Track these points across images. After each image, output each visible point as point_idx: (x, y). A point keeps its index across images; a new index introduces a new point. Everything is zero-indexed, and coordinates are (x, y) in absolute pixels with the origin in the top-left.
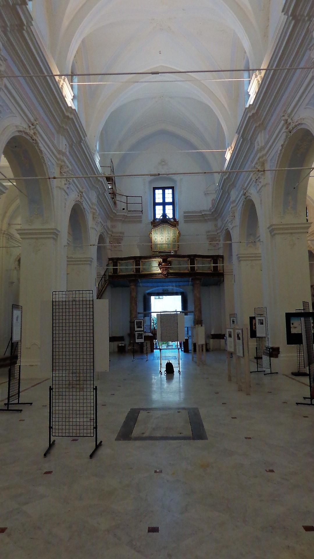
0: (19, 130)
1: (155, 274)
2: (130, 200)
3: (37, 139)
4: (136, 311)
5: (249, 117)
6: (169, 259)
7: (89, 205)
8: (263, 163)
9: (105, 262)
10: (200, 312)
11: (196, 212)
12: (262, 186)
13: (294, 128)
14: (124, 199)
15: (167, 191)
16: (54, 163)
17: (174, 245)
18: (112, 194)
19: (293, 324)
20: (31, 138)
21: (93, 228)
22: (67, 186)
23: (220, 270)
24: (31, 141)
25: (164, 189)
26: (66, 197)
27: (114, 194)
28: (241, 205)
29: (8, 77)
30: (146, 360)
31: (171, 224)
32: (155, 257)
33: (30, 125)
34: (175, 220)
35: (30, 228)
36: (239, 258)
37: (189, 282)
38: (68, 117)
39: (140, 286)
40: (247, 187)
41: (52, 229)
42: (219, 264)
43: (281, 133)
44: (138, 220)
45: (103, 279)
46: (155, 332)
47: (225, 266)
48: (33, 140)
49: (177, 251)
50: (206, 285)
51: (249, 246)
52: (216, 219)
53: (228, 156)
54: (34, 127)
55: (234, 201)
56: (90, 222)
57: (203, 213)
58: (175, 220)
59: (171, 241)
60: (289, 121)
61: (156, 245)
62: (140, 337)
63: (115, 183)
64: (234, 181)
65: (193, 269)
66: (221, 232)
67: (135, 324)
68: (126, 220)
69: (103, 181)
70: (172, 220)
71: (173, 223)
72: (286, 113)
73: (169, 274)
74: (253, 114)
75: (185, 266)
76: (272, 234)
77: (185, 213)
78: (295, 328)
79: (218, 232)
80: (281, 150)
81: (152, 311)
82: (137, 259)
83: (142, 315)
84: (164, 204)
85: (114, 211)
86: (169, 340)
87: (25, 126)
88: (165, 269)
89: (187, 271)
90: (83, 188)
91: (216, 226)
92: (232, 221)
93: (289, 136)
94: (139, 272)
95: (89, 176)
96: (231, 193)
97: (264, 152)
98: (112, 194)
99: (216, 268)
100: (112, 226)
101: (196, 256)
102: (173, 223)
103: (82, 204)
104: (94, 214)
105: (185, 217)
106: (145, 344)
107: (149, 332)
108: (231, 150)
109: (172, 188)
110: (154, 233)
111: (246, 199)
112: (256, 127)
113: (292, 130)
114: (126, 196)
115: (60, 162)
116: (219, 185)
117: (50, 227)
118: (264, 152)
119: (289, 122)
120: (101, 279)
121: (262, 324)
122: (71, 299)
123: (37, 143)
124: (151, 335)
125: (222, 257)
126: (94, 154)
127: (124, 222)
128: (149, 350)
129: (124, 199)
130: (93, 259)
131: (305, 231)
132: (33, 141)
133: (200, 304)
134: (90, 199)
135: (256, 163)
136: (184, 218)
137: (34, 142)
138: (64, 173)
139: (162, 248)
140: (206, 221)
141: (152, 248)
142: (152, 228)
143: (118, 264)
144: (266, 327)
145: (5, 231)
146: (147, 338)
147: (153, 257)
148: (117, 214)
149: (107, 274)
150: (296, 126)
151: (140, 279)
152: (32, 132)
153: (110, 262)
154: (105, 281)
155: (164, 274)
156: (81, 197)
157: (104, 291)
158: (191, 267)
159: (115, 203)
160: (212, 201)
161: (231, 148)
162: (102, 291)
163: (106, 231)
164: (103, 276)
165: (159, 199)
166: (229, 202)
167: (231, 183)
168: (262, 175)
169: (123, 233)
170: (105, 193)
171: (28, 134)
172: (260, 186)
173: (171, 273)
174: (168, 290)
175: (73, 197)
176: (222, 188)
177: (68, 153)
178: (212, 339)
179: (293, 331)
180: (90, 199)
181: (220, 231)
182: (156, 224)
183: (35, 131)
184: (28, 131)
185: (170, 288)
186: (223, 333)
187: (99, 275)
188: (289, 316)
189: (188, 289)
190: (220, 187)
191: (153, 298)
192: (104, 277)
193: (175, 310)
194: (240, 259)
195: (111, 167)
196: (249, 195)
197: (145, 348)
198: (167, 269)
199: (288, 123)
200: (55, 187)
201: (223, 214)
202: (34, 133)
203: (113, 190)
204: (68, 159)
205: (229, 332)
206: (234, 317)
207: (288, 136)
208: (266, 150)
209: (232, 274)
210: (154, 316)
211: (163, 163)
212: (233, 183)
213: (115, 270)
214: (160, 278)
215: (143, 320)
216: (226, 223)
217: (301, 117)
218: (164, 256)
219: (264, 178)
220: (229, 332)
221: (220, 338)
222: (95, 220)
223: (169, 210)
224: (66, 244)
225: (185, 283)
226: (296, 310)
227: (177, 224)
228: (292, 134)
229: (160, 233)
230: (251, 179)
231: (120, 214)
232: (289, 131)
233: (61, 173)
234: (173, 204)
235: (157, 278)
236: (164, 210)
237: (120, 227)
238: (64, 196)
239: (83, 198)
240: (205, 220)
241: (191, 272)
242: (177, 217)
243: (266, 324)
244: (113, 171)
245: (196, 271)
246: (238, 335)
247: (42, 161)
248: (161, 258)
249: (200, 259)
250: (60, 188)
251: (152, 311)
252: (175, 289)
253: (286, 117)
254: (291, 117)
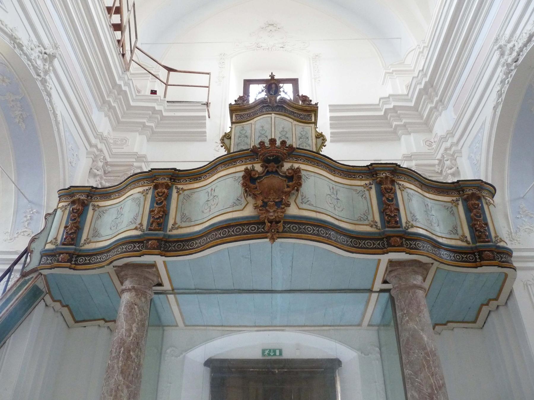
28: (494, 95)
103: (44, 82)
191: (120, 32)
211: (271, 28)
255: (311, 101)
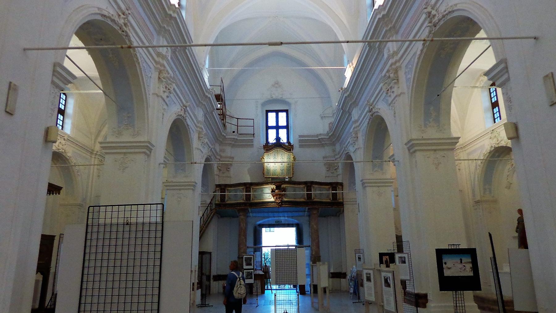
0: (102, 13)
1: (266, 203)
2: (241, 122)
3: (128, 32)
4: (246, 245)
5: (379, 19)
6: (283, 186)
7: (194, 123)
8: (396, 70)
9: (212, 188)
10: (318, 247)
11: (312, 136)
12: (396, 96)
13: (441, 19)
14: (234, 121)
15: (280, 114)
16: (152, 66)
17: (288, 169)
18: (221, 115)
19: (445, 263)
20: (120, 28)
21: (198, 149)
22: (166, 94)
23: (339, 199)
24: (120, 32)
25: (277, 112)
26: (165, 107)
27: (223, 116)
28: (366, 123)
29: (144, 47)
30: (256, 305)
31: (284, 148)
32: (267, 183)
33: (120, 14)
34: (290, 144)
35: (118, 140)
36: (363, 184)
37: (305, 212)
38: (171, 15)
39: (250, 217)
40: (374, 101)
41: (143, 142)
42: (339, 191)
43: (423, 28)
44: (249, 144)
45: (209, 208)
46: (266, 270)
47: (346, 194)
48: (123, 32)
49: (292, 177)
50: (323, 215)
51: (375, 170)
52: (333, 144)
53: (348, 74)
54: (125, 17)
55: (356, 121)
56: (196, 143)
57: (320, 137)
58: (290, 144)
59: (285, 169)
60: (434, 12)
61: (268, 170)
62: (249, 277)
63: (225, 104)
64: (356, 98)
65: (309, 196)
66: (340, 157)
67: (244, 261)
68: (236, 144)
69: (211, 98)
70: (287, 144)
71: (288, 147)
72: (428, 6)
73: (282, 202)
74: (383, 16)
75: (300, 194)
76: (411, 151)
77: (300, 136)
78: (449, 268)
79: (336, 157)
80: (422, 51)
81: (263, 245)
82: (248, 186)
83: (252, 250)
84: (277, 127)
85: (223, 134)
86: (286, 283)
87: (115, 14)
88: (279, 197)
89: (302, 200)
90: (187, 102)
91: (334, 151)
92: (354, 143)
93: (433, 32)
94: (250, 200)
95: (177, 44)
96: (352, 113)
97: (396, 58)
98: (221, 115)
99: (335, 195)
100: (221, 151)
101: (312, 183)
102: (288, 147)
103: (186, 120)
104: (199, 133)
105: (300, 141)
106: (254, 285)
107: (260, 270)
108: (352, 67)
109: (287, 111)
110: (267, 158)
111: (372, 116)
112: (386, 31)
113: (437, 23)
114: (237, 118)
115: (159, 66)
116: (339, 105)
117: (143, 140)
118: (396, 58)
119: (434, 14)
120: (207, 208)
121: (404, 262)
122: (121, 221)
123: (127, 35)
124: (261, 273)
125: (341, 184)
126: (202, 69)
127: (233, 146)
128: (259, 291)
129: (234, 121)
130: (196, 183)
131: (450, 147)
132: (123, 33)
133: (318, 237)
134: (195, 115)
135: (388, 71)
136: (300, 142)
137: (123, 35)
138: (163, 79)
139: (275, 174)
140: (323, 146)
141: (264, 174)
142: (265, 153)
143: (226, 191)
144: (409, 267)
145: (97, 152)
146: (257, 277)
147: (265, 183)
148: (227, 137)
149: (213, 202)
150: (444, 16)
151: (250, 208)
152: (121, 22)
153: (217, 189)
154: (211, 210)
155: (278, 203)
156: (185, 111)
157: (209, 223)
158: (307, 193)
159: (224, 125)
160: (330, 124)
161: (353, 64)
162: (207, 221)
163: (214, 154)
164: (209, 205)
165: (272, 122)
166: (351, 122)
167: (353, 101)
168: (395, 83)
169: (233, 158)
170: (213, 112)
171: (116, 23)
172: (393, 96)
173: (285, 201)
174: (281, 221)
175: (174, 111)
176: (342, 108)
177: (169, 58)
178: (331, 278)
179: (447, 273)
180: (195, 115)
181: (339, 156)
182: (268, 147)
183: (126, 22)
184: (116, 19)
185: (283, 219)
186: (344, 271)
187: (203, 204)
188: (440, 253)
189: (304, 221)
190: (339, 107)
191: (264, 230)
192: (211, 206)
193: (286, 244)
194: (366, 185)
195: (221, 86)
196: (376, 111)
197: (254, 290)
198: (280, 196)
199: (431, 16)
200: (151, 93)
201: (343, 137)
202: (125, 25)
203: (223, 111)
204: (169, 64)
205: (367, 274)
206: (359, 253)
207: (433, 31)
208: (399, 55)
209: (356, 204)
210: (266, 251)
211: (276, 85)
212: (355, 101)
213: (223, 197)
214: (273, 207)
215: (253, 256)
216: (347, 146)
217: (450, 5)
218: (277, 182)
219: (398, 86)
220: (367, 274)
221: (340, 278)
222: (201, 140)
223: (283, 134)
224: (162, 162)
225: (301, 214)
226: (449, 245)
227: (291, 148)
228: (438, 27)
229: (270, 171)
230: (381, 89)
231: (231, 137)
232: (434, 25)
233: (159, 78)
234: (287, 127)
235: (270, 207)
236: (277, 133)
237: (229, 151)
238: (162, 106)
239: (186, 113)
240: (322, 144)
241: (308, 201)
242: (292, 141)
243: (409, 262)
244: (223, 90)
245: (313, 200)
246: (386, 281)
247: (135, 59)
248: (274, 184)
249: (317, 186)
250: (158, 96)
251: (263, 245)
252: (291, 221)
253: (429, 9)
254: (435, 9)
255: (291, 144)
